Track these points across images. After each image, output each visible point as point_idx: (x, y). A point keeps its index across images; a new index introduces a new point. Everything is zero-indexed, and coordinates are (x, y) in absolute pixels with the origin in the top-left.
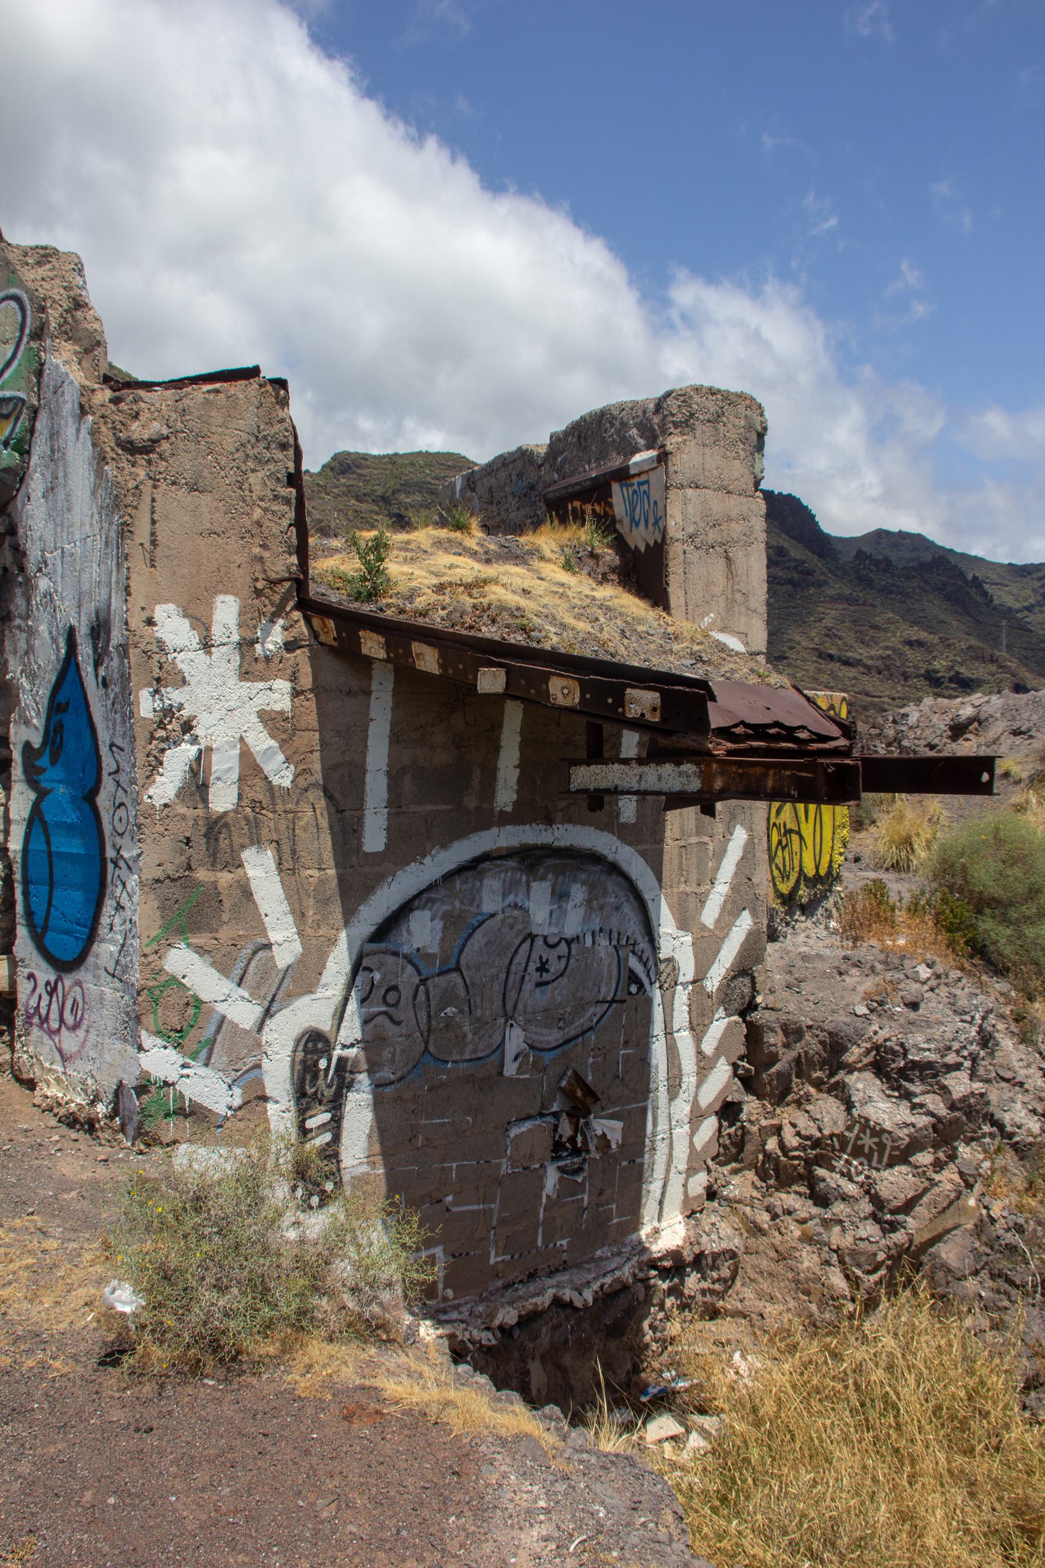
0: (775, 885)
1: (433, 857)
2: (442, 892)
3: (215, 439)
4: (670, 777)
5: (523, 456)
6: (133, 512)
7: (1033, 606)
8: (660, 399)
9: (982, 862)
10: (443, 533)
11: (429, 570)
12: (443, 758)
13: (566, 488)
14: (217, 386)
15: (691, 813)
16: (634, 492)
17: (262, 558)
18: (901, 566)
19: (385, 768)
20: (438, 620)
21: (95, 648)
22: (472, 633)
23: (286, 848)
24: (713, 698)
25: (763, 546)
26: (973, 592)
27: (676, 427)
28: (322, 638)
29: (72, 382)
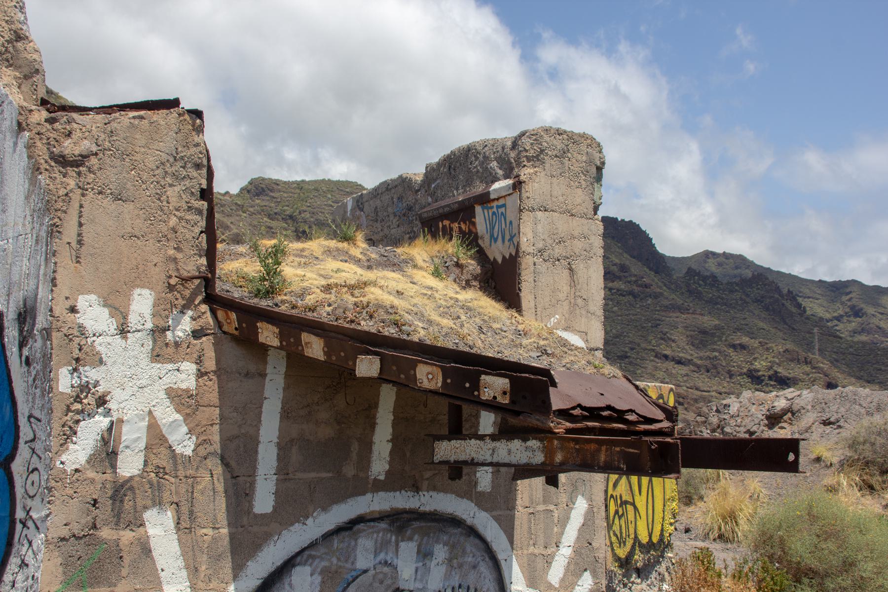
0: (613, 550)
1: (315, 518)
2: (322, 550)
3: (138, 157)
4: (518, 451)
5: (403, 182)
6: (63, 216)
7: (842, 316)
8: (516, 138)
9: (798, 536)
10: (333, 244)
11: (319, 274)
12: (326, 432)
13: (438, 209)
14: (142, 113)
15: (539, 482)
16: (494, 213)
17: (176, 259)
18: (725, 282)
19: (276, 440)
20: (325, 314)
21: (21, 331)
22: (353, 326)
23: (185, 509)
24: (554, 385)
25: (600, 260)
26: (788, 304)
27: (529, 161)
28: (226, 328)
29: (11, 102)
